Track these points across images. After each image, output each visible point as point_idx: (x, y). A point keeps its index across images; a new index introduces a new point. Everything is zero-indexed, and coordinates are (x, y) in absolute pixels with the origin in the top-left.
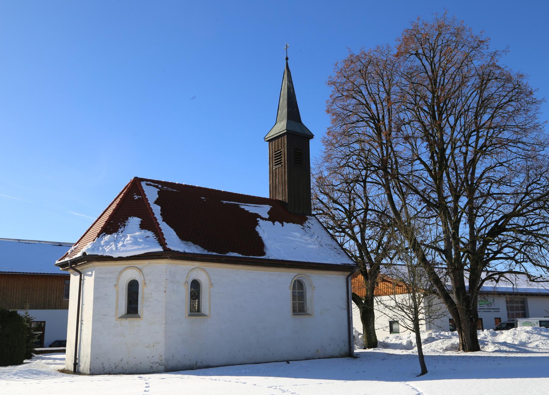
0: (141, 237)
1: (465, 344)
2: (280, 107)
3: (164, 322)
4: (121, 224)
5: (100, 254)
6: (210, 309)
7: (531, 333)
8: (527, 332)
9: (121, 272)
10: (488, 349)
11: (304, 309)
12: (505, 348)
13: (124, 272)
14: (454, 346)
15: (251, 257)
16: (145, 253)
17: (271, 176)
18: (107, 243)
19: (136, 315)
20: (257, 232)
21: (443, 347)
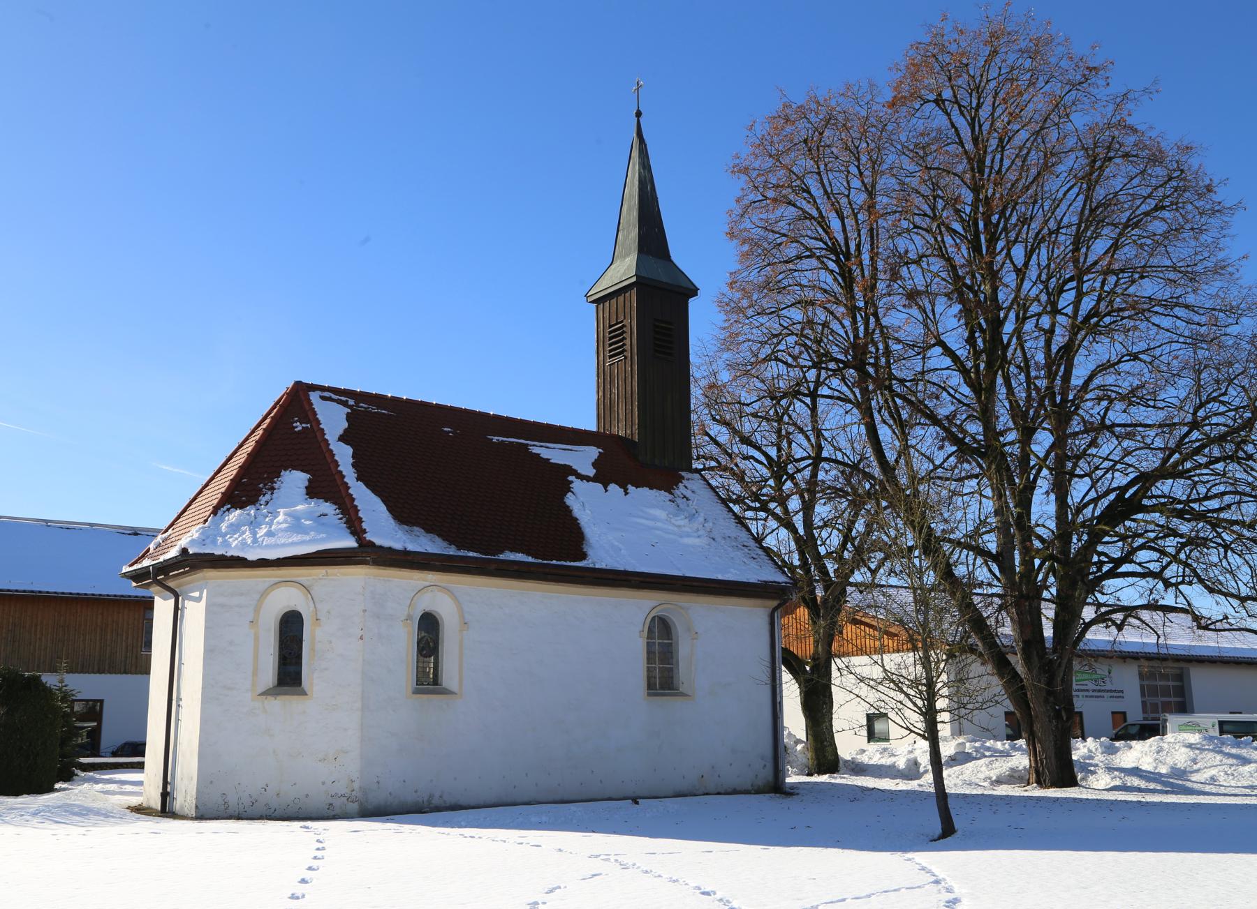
3: (359, 705)
4: (265, 485)
5: (218, 552)
7: (1198, 749)
8: (1190, 746)
9: (264, 594)
12: (1136, 782)
15: (554, 562)
16: (318, 552)
17: (601, 381)
20: (568, 507)
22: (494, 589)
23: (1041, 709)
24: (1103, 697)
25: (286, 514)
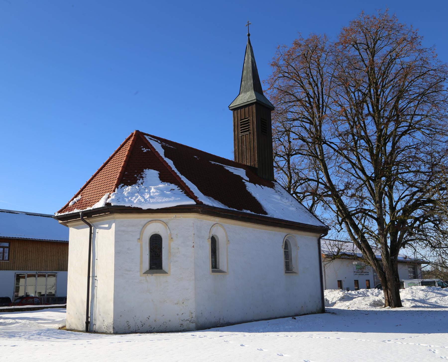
0: (167, 189)
1: (391, 301)
2: (243, 79)
3: (193, 277)
4: (138, 175)
5: (127, 205)
6: (228, 266)
7: (426, 291)
8: (423, 290)
9: (145, 226)
10: (405, 305)
11: (289, 268)
12: (420, 304)
14: (375, 303)
15: (261, 215)
16: (177, 206)
17: (237, 142)
18: (132, 194)
19: (161, 270)
20: (249, 192)
21: (367, 303)
22: (237, 226)
23: (391, 278)
24: (363, 274)
25: (155, 189)
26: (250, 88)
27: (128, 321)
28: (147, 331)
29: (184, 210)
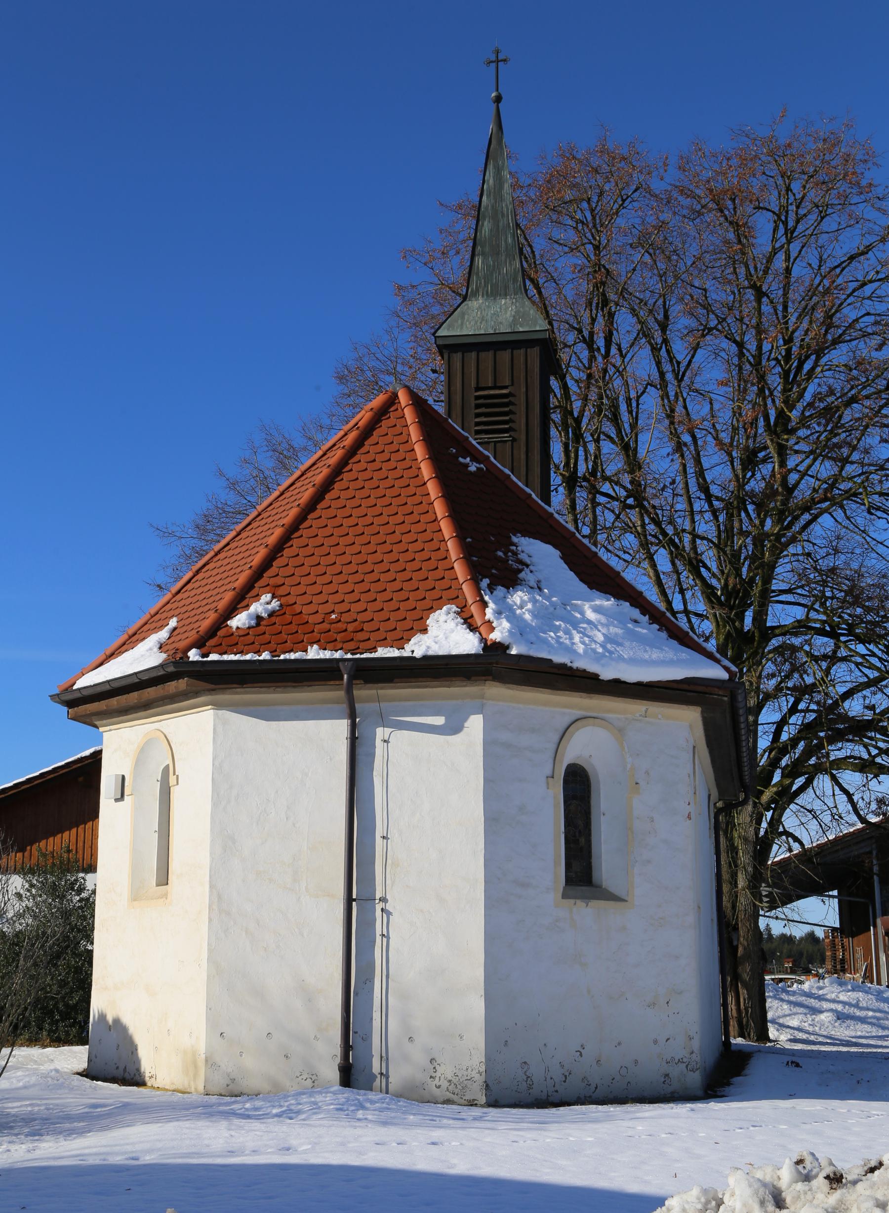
1: (748, 1021)
13: (577, 733)
26: (511, 286)
27: (525, 1063)
28: (579, 1098)
29: (689, 694)
